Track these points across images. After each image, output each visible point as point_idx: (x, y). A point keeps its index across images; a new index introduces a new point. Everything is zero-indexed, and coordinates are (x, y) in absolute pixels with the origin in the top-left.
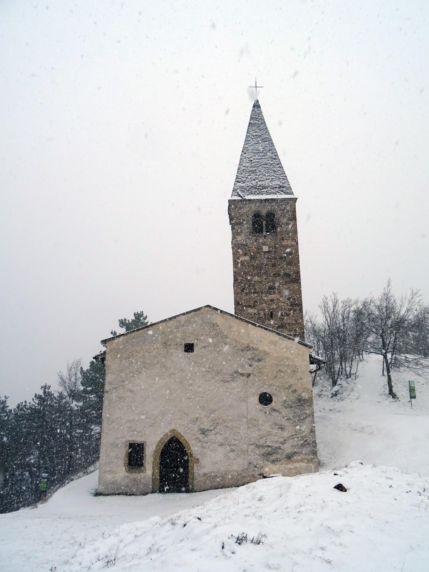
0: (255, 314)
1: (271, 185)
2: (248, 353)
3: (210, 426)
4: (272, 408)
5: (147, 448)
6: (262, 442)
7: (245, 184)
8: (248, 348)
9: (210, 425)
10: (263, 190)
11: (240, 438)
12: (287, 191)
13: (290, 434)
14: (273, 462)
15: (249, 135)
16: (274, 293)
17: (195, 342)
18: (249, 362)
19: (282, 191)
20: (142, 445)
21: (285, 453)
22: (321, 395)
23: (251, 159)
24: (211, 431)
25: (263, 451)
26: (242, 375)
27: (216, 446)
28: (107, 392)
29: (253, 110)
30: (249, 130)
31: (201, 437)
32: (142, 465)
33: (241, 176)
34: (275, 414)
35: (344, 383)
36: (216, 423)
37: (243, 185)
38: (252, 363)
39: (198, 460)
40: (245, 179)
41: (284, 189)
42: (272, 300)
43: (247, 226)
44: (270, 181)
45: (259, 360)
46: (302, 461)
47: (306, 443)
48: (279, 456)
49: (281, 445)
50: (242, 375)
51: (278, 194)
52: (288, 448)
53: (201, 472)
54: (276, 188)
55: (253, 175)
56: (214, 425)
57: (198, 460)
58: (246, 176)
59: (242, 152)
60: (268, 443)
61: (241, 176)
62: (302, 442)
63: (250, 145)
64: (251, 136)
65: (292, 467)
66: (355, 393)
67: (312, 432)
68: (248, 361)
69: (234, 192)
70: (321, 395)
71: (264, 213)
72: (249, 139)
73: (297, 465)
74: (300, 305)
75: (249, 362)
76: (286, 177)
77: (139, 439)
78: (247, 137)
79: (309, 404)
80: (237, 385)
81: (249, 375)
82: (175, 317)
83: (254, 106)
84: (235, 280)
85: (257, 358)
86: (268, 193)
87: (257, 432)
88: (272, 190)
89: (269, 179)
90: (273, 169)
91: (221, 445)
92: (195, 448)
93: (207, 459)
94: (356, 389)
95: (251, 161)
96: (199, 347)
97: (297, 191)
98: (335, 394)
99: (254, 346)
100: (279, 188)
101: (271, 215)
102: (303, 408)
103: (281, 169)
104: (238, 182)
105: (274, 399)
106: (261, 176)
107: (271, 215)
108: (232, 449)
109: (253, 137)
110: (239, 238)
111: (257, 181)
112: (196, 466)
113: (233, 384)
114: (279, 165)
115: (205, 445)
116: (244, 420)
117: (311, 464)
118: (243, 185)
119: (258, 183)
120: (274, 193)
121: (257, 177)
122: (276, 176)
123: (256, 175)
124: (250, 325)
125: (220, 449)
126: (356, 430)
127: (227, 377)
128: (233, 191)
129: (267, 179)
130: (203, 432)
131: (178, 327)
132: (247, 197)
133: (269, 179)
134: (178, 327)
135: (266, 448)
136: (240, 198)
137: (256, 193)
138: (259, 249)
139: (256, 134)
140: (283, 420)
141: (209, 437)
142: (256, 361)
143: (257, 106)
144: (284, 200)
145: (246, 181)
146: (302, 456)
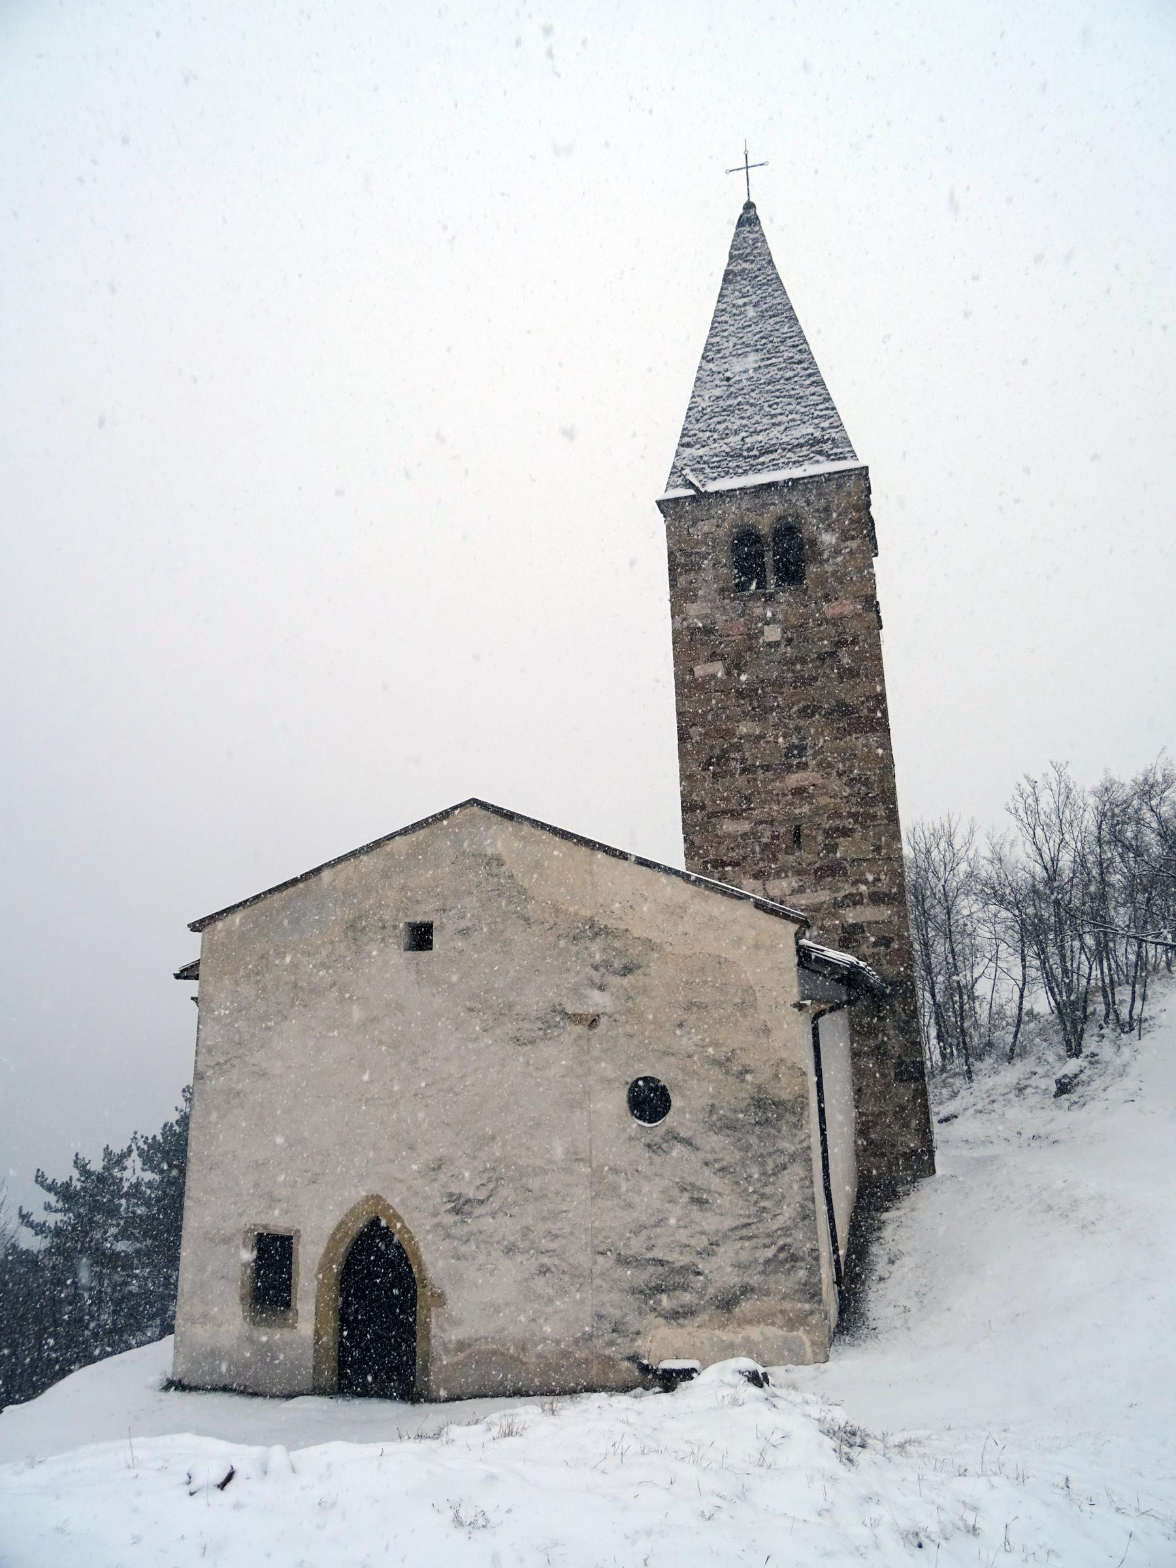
0: (744, 835)
1: (786, 439)
2: (594, 947)
3: (478, 1188)
4: (668, 1132)
5: (301, 1250)
6: (636, 1246)
7: (706, 449)
8: (598, 932)
9: (478, 1182)
10: (761, 460)
11: (567, 1229)
12: (835, 450)
13: (729, 1223)
14: (675, 1316)
15: (724, 306)
16: (803, 766)
17: (436, 919)
18: (596, 977)
19: (820, 453)
20: (291, 1238)
21: (711, 1291)
22: (1026, 1087)
23: (728, 374)
24: (481, 1202)
25: (645, 1276)
26: (575, 1018)
27: (497, 1254)
28: (627, 1083)
29: (737, 235)
30: (725, 292)
31: (450, 1219)
32: (288, 1305)
33: (698, 426)
34: (678, 1150)
35: (1106, 1051)
36: (493, 1178)
37: (701, 452)
38: (605, 981)
39: (440, 1295)
40: (708, 434)
41: (826, 447)
42: (799, 792)
43: (716, 570)
44: (782, 428)
45: (627, 970)
46: (762, 1318)
47: (782, 1256)
48: (687, 1298)
49: (697, 1260)
50: (575, 1018)
51: (806, 465)
52: (722, 1271)
53: (454, 1335)
54: (801, 445)
55: (733, 420)
56: (491, 1186)
57: (440, 1295)
58: (712, 427)
59: (703, 358)
60: (658, 1254)
61: (698, 426)
62: (770, 1253)
63: (726, 334)
64: (729, 309)
65: (738, 1339)
66: (1129, 1083)
67: (804, 1218)
68: (592, 972)
69: (674, 478)
70: (1026, 1087)
71: (765, 524)
72: (723, 318)
73: (754, 1333)
74: (889, 797)
75: (596, 977)
76: (834, 409)
77: (277, 1221)
78: (719, 312)
79: (794, 1119)
80: (558, 1054)
81: (593, 1022)
82: (377, 844)
83: (740, 224)
84: (683, 736)
85: (617, 964)
86: (777, 467)
87: (620, 1213)
88: (789, 455)
89: (779, 424)
90: (793, 392)
91: (510, 1250)
92: (434, 1260)
93: (470, 1299)
94: (1134, 1070)
95: (728, 379)
96: (450, 929)
97: (869, 445)
98: (1064, 1087)
99: (611, 923)
100: (812, 445)
101: (788, 531)
102: (773, 1131)
103: (818, 389)
104: (688, 445)
105: (676, 1102)
106: (757, 418)
107: (788, 531)
108: (543, 1265)
109: (735, 311)
110: (693, 609)
111: (744, 434)
112: (438, 1316)
113: (548, 1050)
114: (813, 379)
115: (463, 1249)
116: (584, 1169)
117: (801, 1333)
118: (701, 452)
119: (747, 440)
120: (794, 463)
121: (745, 422)
122: (803, 410)
123: (743, 418)
124: (600, 855)
125: (505, 1264)
126: (1050, 1208)
127: (527, 1025)
128: (672, 473)
129: (774, 424)
130: (460, 1206)
131: (386, 875)
132: (712, 487)
133: (779, 424)
134: (386, 875)
135: (651, 1269)
136: (692, 492)
137: (740, 471)
138: (752, 636)
139: (746, 300)
140: (707, 1172)
141: (472, 1224)
142: (615, 973)
143: (749, 218)
144: (830, 476)
145: (710, 441)
146: (771, 1303)
